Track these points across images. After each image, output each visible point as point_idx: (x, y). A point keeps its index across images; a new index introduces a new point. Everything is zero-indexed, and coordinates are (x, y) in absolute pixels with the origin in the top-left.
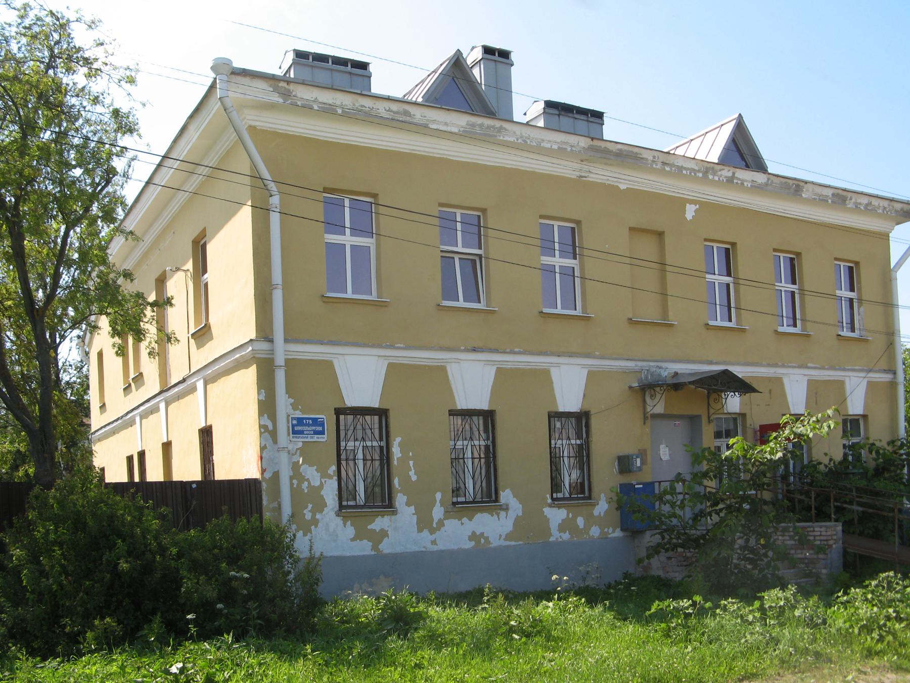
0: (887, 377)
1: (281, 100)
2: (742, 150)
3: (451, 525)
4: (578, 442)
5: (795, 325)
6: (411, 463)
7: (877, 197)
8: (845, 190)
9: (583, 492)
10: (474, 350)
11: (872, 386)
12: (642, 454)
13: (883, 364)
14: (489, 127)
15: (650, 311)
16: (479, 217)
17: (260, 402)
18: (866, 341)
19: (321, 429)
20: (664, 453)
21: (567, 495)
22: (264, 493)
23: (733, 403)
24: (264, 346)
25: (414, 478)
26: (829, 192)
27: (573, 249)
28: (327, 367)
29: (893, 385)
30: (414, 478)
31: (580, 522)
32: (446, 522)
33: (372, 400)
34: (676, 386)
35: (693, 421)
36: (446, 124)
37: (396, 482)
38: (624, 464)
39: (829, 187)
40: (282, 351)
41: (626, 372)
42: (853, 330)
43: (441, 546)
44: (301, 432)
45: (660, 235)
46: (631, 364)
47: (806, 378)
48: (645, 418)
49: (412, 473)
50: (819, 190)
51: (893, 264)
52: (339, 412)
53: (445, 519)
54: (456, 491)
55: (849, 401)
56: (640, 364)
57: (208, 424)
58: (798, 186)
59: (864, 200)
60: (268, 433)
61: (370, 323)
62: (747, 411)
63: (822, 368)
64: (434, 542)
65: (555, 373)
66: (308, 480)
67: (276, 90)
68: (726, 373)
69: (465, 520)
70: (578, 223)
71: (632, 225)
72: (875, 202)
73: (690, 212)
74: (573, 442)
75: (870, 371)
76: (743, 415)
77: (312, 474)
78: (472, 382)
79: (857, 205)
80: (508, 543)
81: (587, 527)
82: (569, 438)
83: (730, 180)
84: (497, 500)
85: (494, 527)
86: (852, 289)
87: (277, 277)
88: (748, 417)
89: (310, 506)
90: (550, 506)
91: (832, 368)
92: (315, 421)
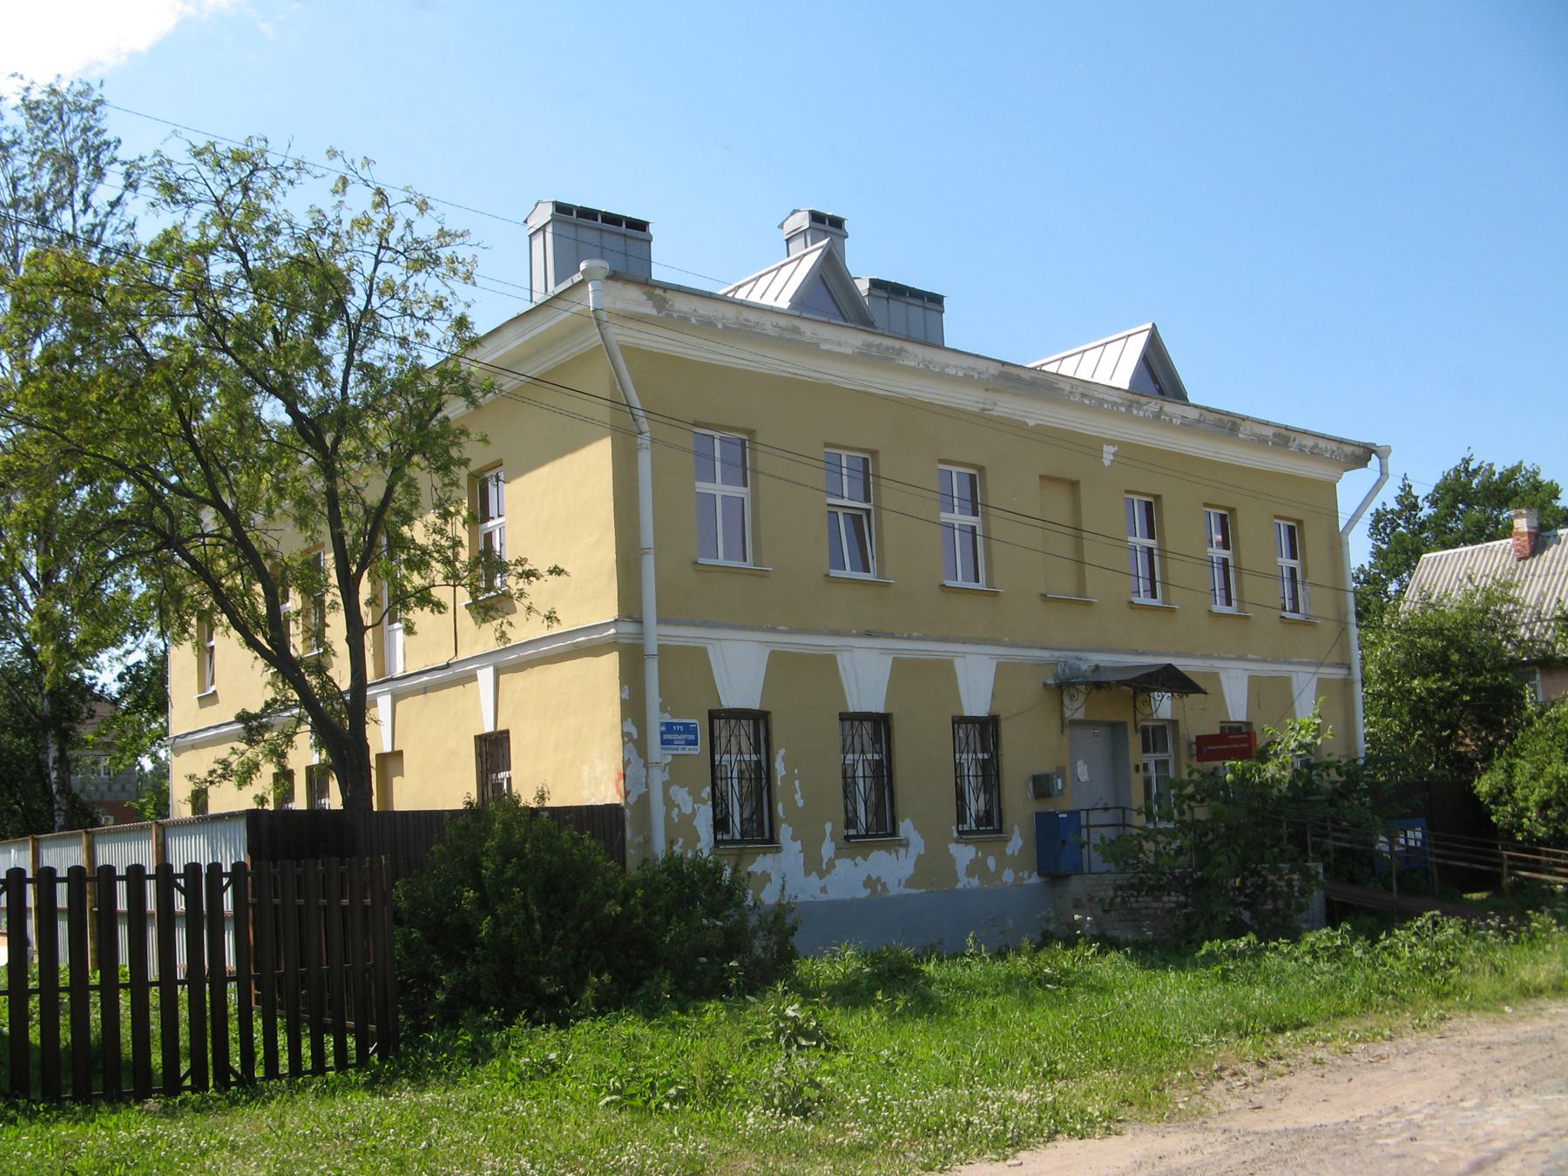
0: (1339, 673)
1: (654, 312)
2: (1157, 373)
3: (843, 865)
4: (876, 757)
5: (867, 570)
6: (797, 783)
7: (1323, 437)
8: (1286, 428)
9: (991, 824)
10: (869, 634)
11: (1323, 686)
12: (1061, 772)
13: (1335, 657)
14: (887, 349)
15: (1064, 586)
16: (865, 461)
17: (623, 701)
18: (1313, 624)
19: (692, 737)
20: (1082, 771)
21: (738, 836)
22: (627, 824)
23: (1164, 705)
24: (629, 628)
25: (800, 803)
26: (1269, 432)
27: (742, 471)
28: (700, 656)
29: (1347, 683)
30: (800, 803)
31: (991, 863)
32: (837, 862)
33: (752, 702)
34: (1098, 684)
35: (1116, 729)
36: (840, 344)
37: (780, 807)
38: (1042, 786)
39: (1267, 424)
40: (656, 635)
41: (1039, 664)
42: (1154, 596)
43: (833, 894)
44: (671, 742)
45: (1074, 485)
46: (1046, 654)
47: (1247, 674)
48: (1063, 726)
49: (798, 796)
50: (1259, 429)
51: (1342, 524)
52: (714, 715)
53: (837, 856)
54: (850, 822)
55: (1297, 704)
56: (1056, 654)
57: (501, 727)
58: (1234, 423)
59: (1309, 442)
60: (635, 743)
61: (744, 597)
62: (1180, 718)
63: (1264, 661)
64: (823, 890)
65: (959, 665)
66: (678, 806)
67: (650, 297)
68: (1169, 668)
69: (859, 859)
70: (981, 469)
71: (1046, 472)
72: (1322, 444)
73: (1108, 453)
74: (869, 756)
75: (1320, 665)
76: (1174, 723)
77: (681, 795)
78: (866, 677)
79: (1301, 449)
80: (908, 891)
81: (999, 871)
82: (740, 751)
83: (1157, 416)
84: (894, 833)
85: (891, 868)
86: (1151, 536)
87: (648, 537)
88: (1181, 723)
89: (681, 840)
90: (957, 842)
91: (1275, 661)
92: (686, 725)
